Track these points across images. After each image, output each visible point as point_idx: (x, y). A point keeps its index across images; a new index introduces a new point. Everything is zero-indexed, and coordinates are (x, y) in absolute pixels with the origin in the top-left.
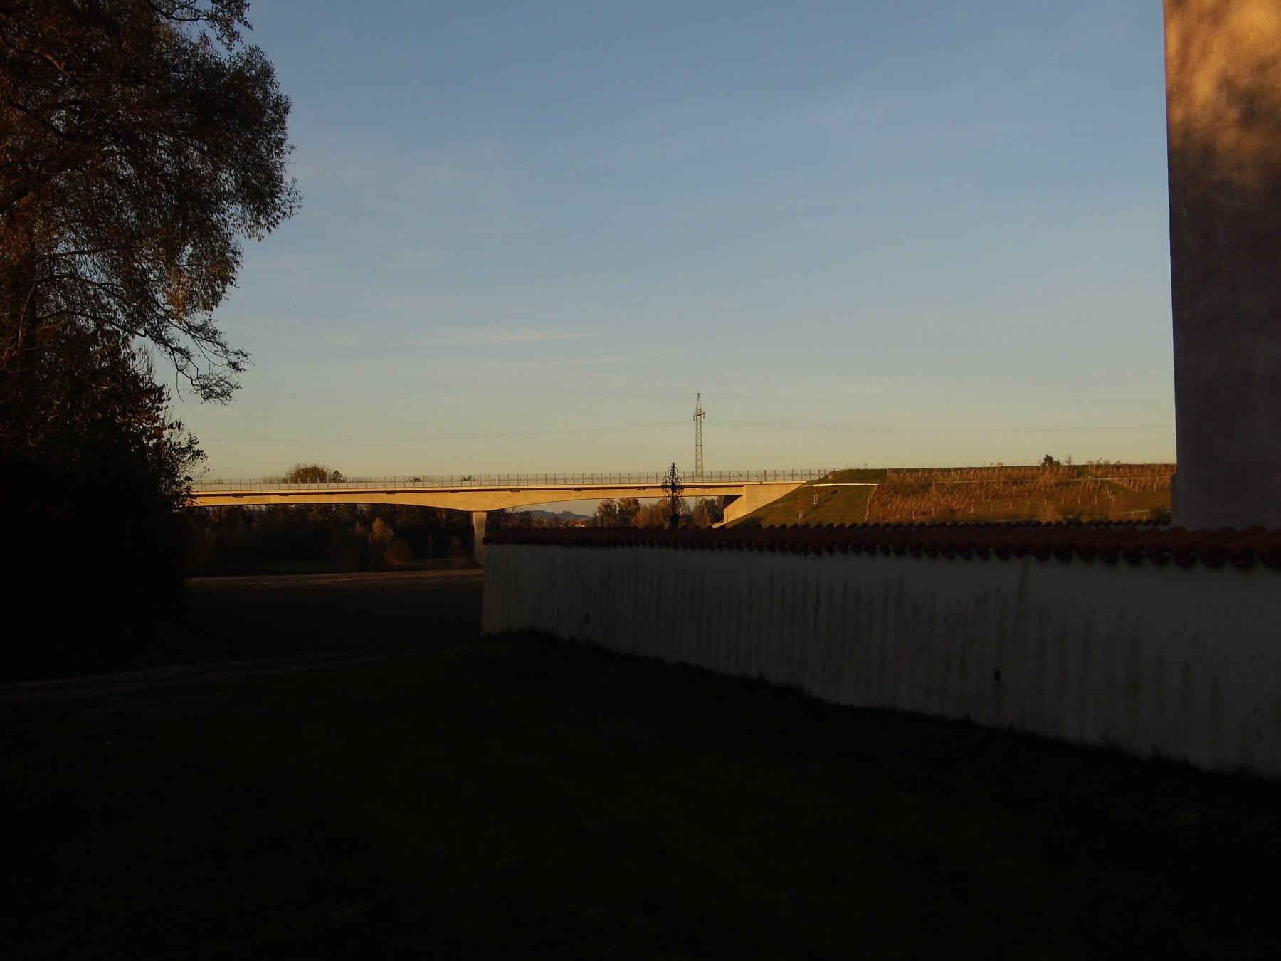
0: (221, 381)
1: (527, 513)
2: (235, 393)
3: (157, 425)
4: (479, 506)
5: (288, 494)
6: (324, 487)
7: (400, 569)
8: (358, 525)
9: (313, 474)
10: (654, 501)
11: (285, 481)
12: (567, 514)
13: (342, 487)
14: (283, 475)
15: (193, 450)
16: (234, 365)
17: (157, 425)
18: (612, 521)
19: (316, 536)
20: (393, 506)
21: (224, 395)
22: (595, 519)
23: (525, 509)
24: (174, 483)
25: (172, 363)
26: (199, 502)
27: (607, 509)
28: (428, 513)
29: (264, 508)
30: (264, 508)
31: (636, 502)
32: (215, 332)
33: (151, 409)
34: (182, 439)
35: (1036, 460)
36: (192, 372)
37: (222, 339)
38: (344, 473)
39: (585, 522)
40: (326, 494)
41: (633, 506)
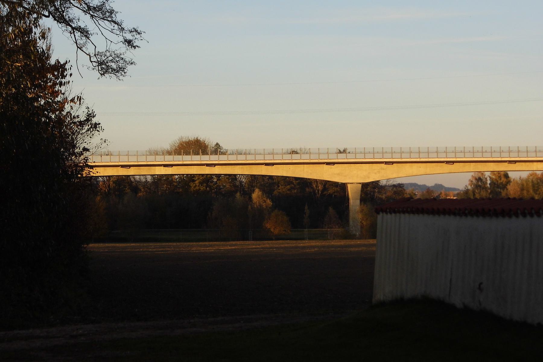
0: (118, 57)
1: (400, 186)
2: (129, 68)
3: (59, 99)
4: (353, 177)
5: (172, 166)
6: (205, 159)
7: (278, 238)
8: (238, 195)
9: (196, 147)
10: (525, 175)
11: (169, 153)
12: (440, 186)
13: (223, 159)
14: (167, 146)
15: (90, 123)
16: (129, 43)
17: (59, 99)
18: (484, 194)
19: (195, 204)
20: (271, 177)
21: (119, 70)
22: (467, 192)
23: (399, 181)
24: (74, 154)
25: (71, 41)
26: (95, 172)
27: (479, 181)
28: (304, 183)
29: (149, 179)
30: (149, 179)
31: (506, 176)
32: (112, 12)
33: (55, 84)
34: (80, 113)
35: (433, 184)
36: (90, 49)
37: (118, 18)
38: (225, 146)
39: (458, 194)
40: (208, 165)
41: (503, 180)
